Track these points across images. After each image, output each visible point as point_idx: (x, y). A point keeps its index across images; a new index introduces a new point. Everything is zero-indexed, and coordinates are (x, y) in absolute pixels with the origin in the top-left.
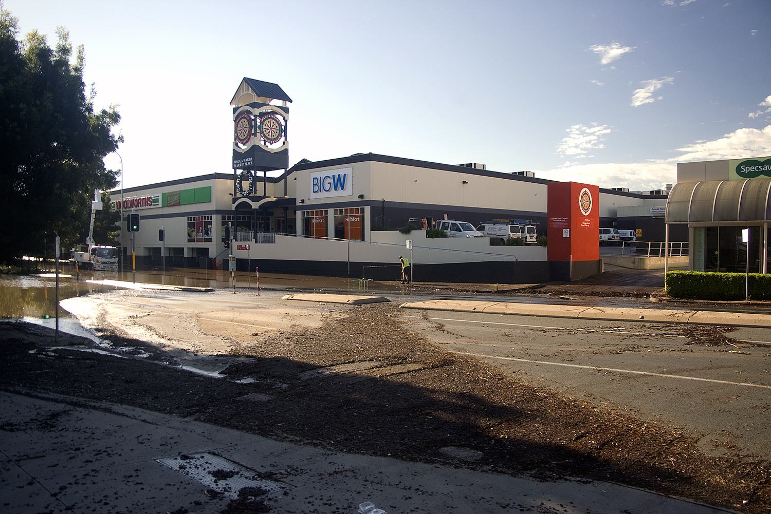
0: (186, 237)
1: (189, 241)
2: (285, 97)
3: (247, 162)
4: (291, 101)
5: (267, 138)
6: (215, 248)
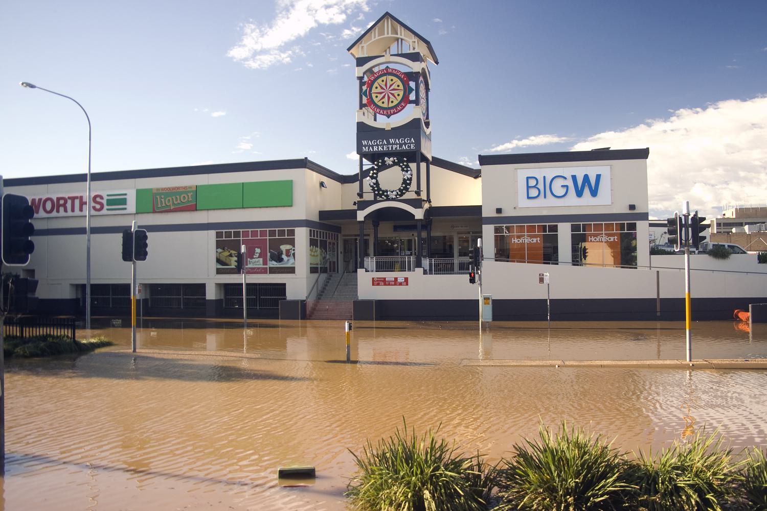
0: (214, 265)
1: (219, 271)
6: (305, 282)
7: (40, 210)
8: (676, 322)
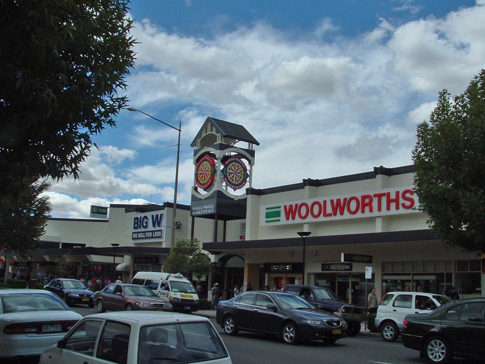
2: (252, 141)
3: (208, 209)
4: (258, 144)
5: (229, 182)
7: (296, 217)
8: (129, 349)
